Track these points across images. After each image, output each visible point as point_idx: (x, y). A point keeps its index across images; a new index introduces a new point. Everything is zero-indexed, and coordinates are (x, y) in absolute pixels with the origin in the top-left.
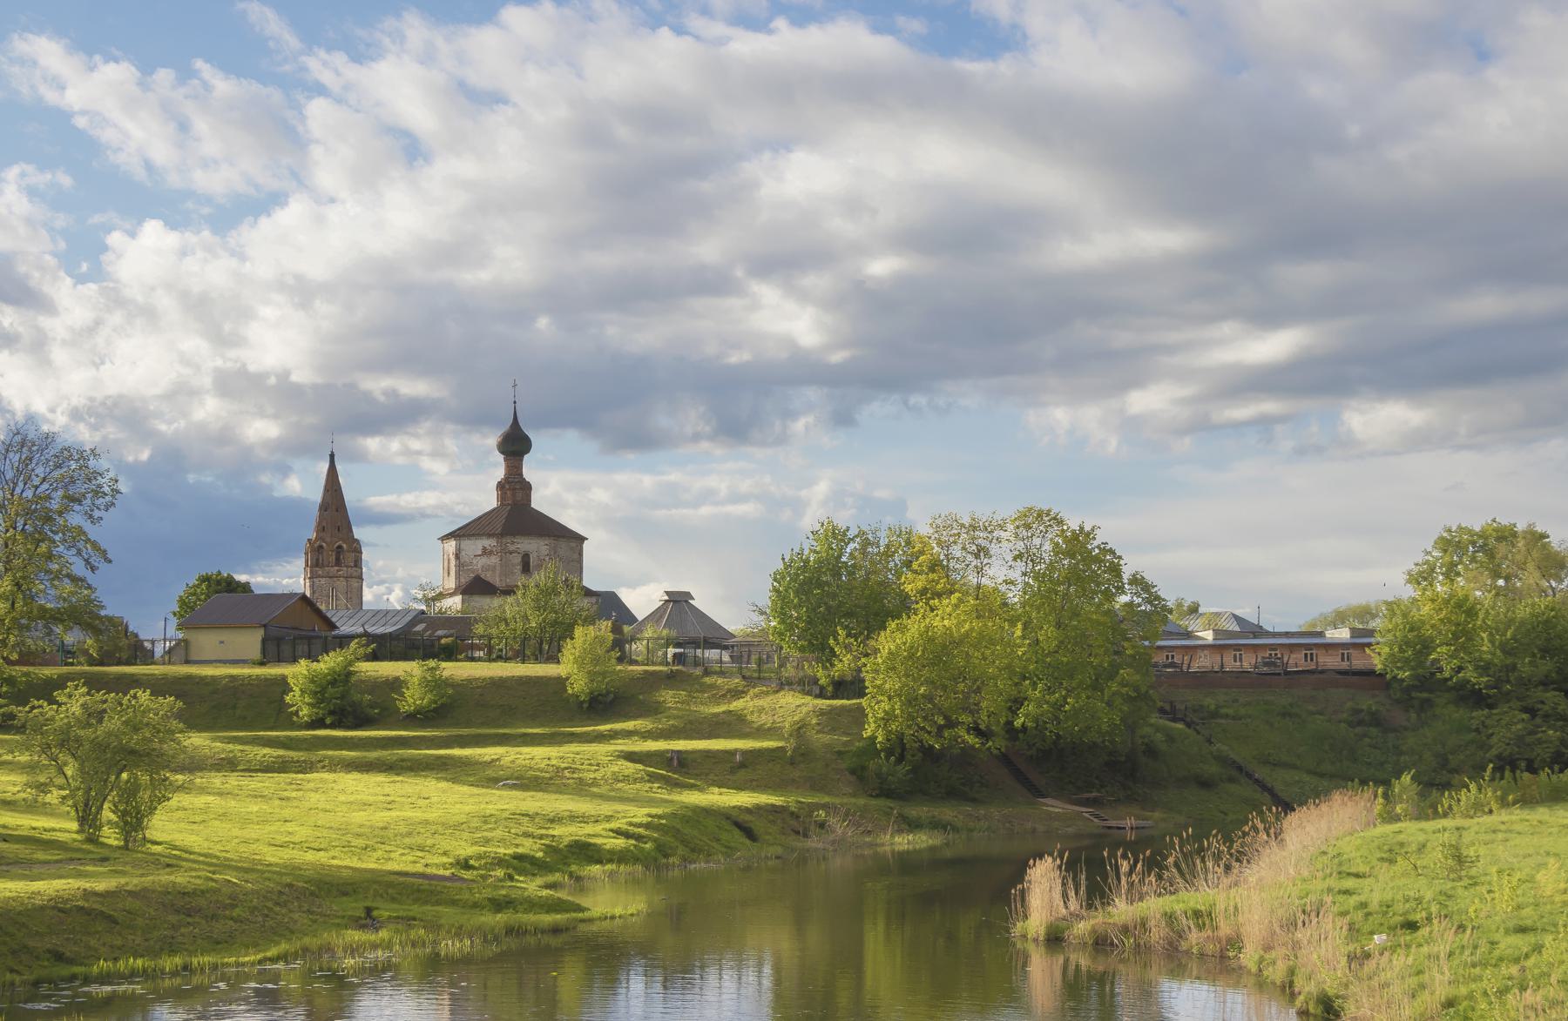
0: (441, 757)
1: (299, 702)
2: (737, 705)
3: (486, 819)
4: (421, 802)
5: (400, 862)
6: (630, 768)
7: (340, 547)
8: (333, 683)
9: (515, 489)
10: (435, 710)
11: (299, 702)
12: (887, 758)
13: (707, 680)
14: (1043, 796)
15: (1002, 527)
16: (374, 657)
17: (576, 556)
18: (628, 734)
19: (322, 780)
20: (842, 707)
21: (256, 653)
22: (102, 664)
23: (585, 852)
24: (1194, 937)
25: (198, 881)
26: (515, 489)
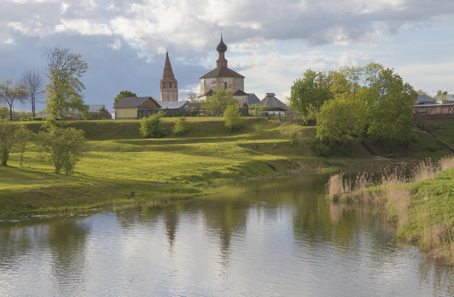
0: (182, 146)
1: (144, 130)
2: (278, 129)
3: (187, 165)
4: (170, 160)
5: (154, 178)
6: (240, 149)
7: (170, 82)
8: (153, 124)
9: (222, 62)
10: (184, 132)
11: (144, 130)
12: (323, 144)
13: (269, 121)
14: (376, 155)
15: (362, 70)
16: (165, 116)
17: (241, 83)
18: (242, 138)
19: (145, 154)
20: (310, 129)
21: (136, 115)
22: (91, 119)
23: (216, 175)
24: (377, 198)
25: (79, 185)
26: (222, 62)
